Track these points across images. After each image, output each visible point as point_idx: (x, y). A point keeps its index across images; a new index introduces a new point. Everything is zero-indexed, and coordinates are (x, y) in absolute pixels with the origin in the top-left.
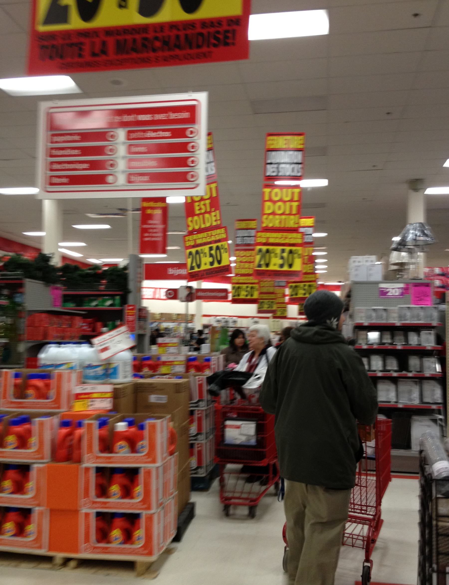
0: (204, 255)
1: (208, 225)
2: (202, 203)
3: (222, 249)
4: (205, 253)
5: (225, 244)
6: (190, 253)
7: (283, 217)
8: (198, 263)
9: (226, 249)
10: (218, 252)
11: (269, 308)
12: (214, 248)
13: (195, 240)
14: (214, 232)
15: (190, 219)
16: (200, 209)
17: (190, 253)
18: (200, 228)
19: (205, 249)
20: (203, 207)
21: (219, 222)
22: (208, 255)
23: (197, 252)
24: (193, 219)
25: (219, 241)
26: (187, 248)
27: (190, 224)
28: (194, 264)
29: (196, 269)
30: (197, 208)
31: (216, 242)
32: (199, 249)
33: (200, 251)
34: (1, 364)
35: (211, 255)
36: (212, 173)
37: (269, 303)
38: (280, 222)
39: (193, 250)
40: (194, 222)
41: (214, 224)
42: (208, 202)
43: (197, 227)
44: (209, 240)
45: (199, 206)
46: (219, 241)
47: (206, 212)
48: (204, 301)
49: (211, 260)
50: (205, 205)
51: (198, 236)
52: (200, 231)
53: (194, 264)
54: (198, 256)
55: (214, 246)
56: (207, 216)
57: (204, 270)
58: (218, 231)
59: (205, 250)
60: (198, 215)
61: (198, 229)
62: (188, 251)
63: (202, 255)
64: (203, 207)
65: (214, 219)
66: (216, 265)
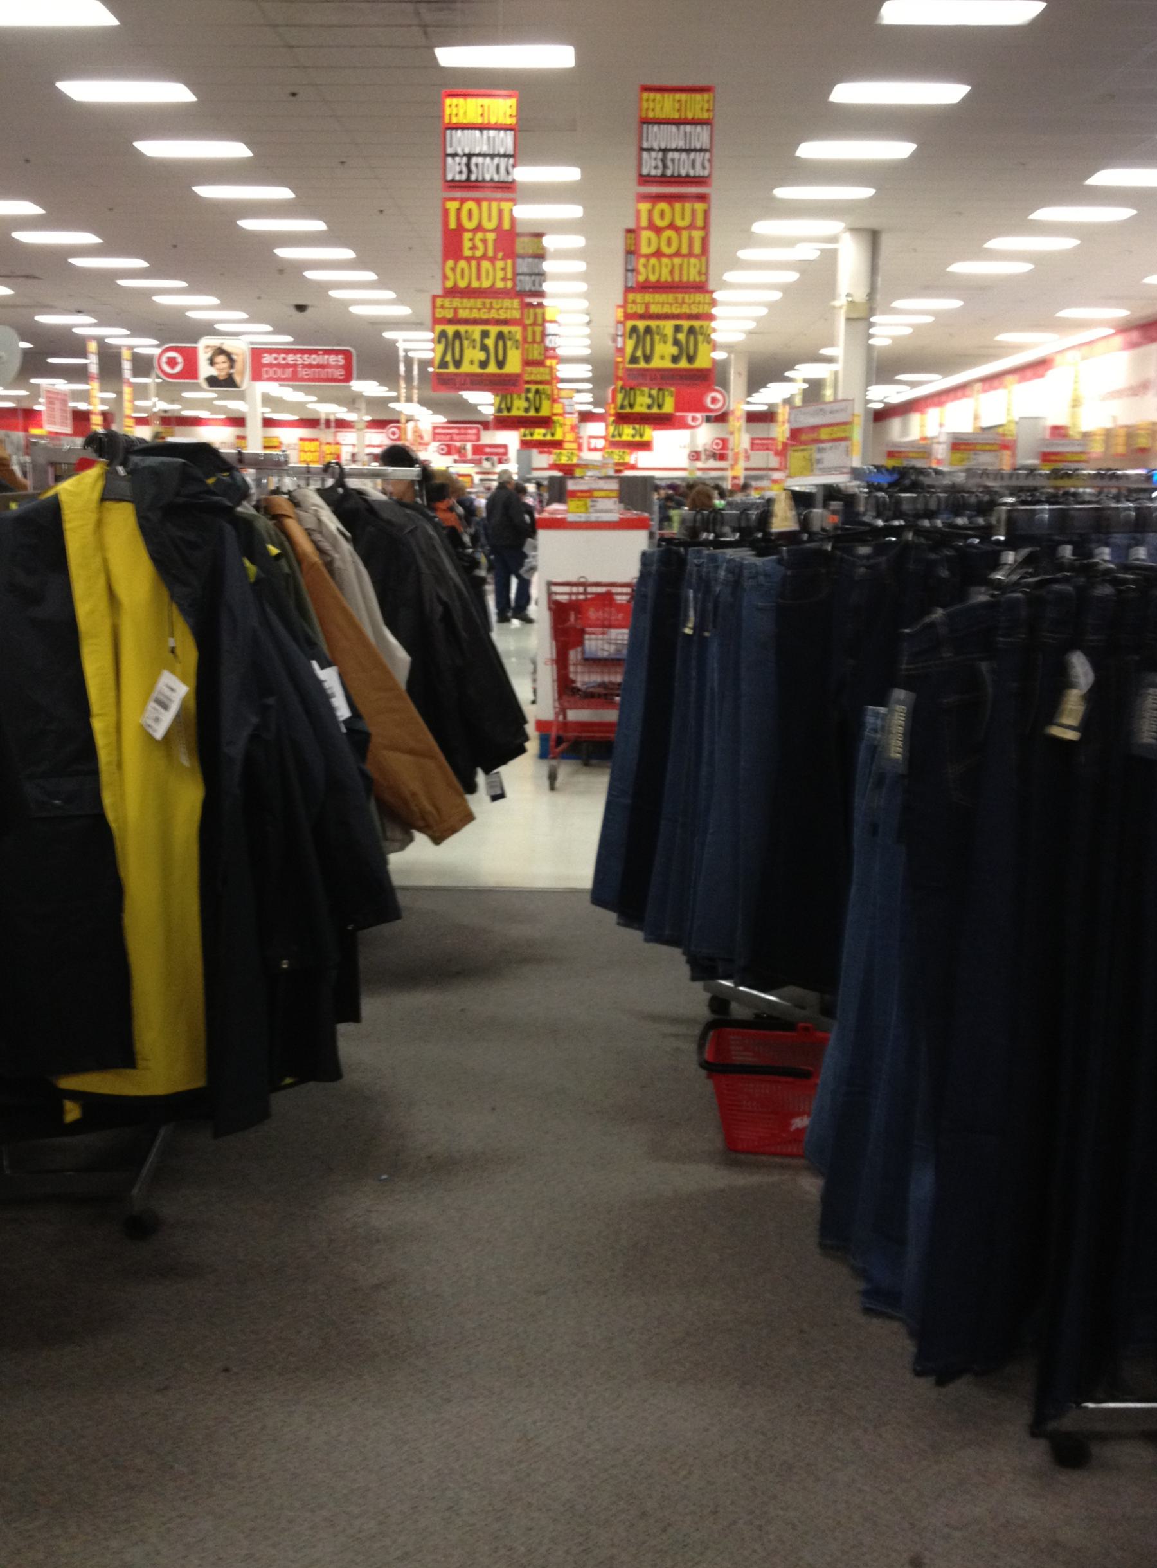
0: (660, 339)
1: (486, 284)
2: (480, 235)
3: (510, 339)
4: (474, 340)
5: (516, 332)
6: (634, 329)
7: (677, 261)
8: (648, 352)
9: (517, 341)
10: (692, 338)
11: (568, 461)
12: (685, 329)
13: (647, 305)
14: (497, 303)
15: (450, 263)
16: (474, 248)
17: (634, 329)
18: (658, 281)
19: (664, 327)
20: (480, 245)
21: (509, 285)
22: (670, 340)
23: (648, 330)
24: (456, 264)
25: (506, 322)
26: (628, 316)
27: (449, 273)
28: (639, 353)
29: (452, 369)
30: (467, 244)
31: (498, 322)
32: (653, 324)
33: (698, 328)
34: (2, 492)
35: (676, 342)
36: (702, 174)
37: (569, 455)
38: (672, 272)
39: (641, 325)
40: (650, 268)
41: (500, 285)
42: (491, 237)
43: (462, 284)
44: (485, 317)
45: (471, 240)
46: (506, 322)
47: (484, 257)
48: (655, 429)
49: (674, 350)
50: (484, 241)
51: (654, 298)
52: (469, 293)
53: (639, 353)
54: (648, 338)
55: (686, 324)
56: (485, 264)
57: (467, 375)
58: (507, 303)
59: (472, 334)
60: (468, 259)
61: (452, 288)
62: (630, 323)
63: (657, 338)
64: (480, 245)
65: (500, 274)
66: (683, 364)
